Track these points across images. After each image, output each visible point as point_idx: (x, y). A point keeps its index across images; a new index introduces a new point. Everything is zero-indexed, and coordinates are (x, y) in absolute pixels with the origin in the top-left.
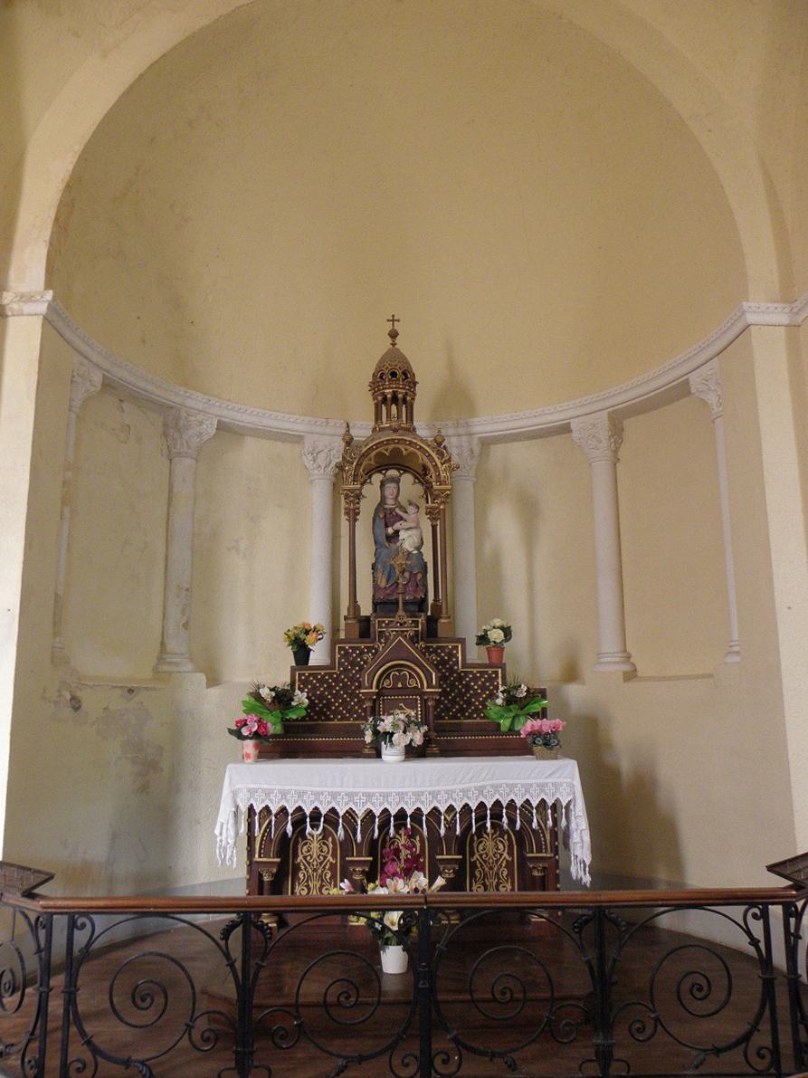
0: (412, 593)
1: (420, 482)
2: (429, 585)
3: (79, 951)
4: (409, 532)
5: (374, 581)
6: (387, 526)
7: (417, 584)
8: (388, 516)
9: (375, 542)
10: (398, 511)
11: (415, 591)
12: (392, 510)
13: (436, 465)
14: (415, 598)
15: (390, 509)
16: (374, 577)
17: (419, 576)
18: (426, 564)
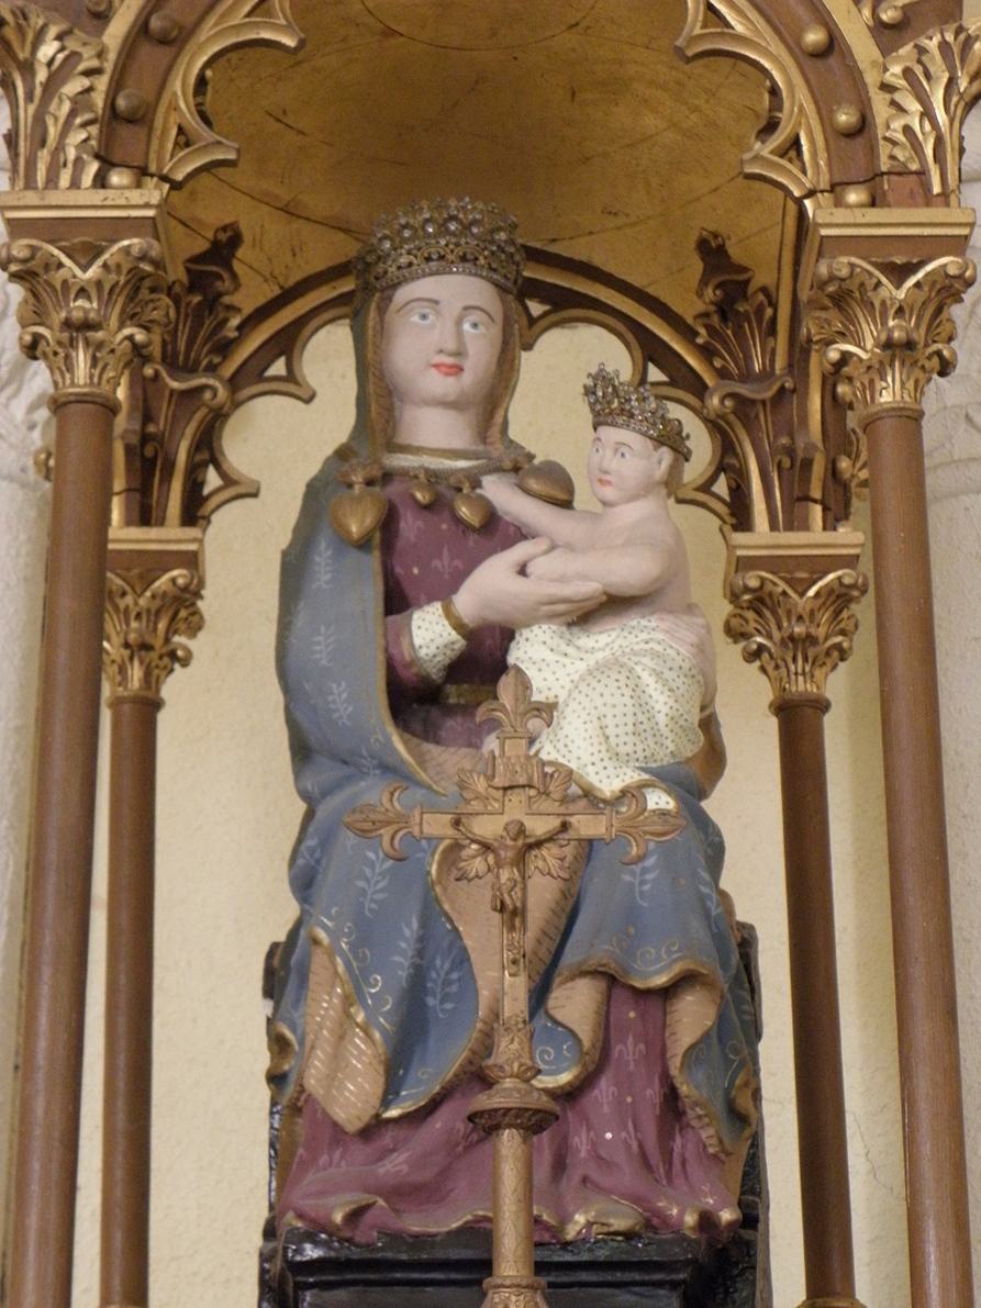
0: (627, 1175)
1: (207, 448)
2: (770, 1123)
3: (417, 675)
4: (606, 640)
5: (276, 1079)
6: (397, 601)
7: (671, 1096)
8: (410, 526)
9: (302, 751)
10: (500, 493)
11: (658, 1162)
12: (442, 495)
13: (833, 45)
14: (653, 1223)
15: (434, 477)
16: (279, 1044)
17: (692, 1017)
18: (746, 943)
